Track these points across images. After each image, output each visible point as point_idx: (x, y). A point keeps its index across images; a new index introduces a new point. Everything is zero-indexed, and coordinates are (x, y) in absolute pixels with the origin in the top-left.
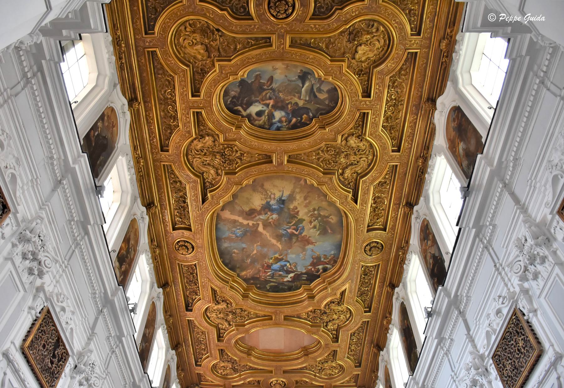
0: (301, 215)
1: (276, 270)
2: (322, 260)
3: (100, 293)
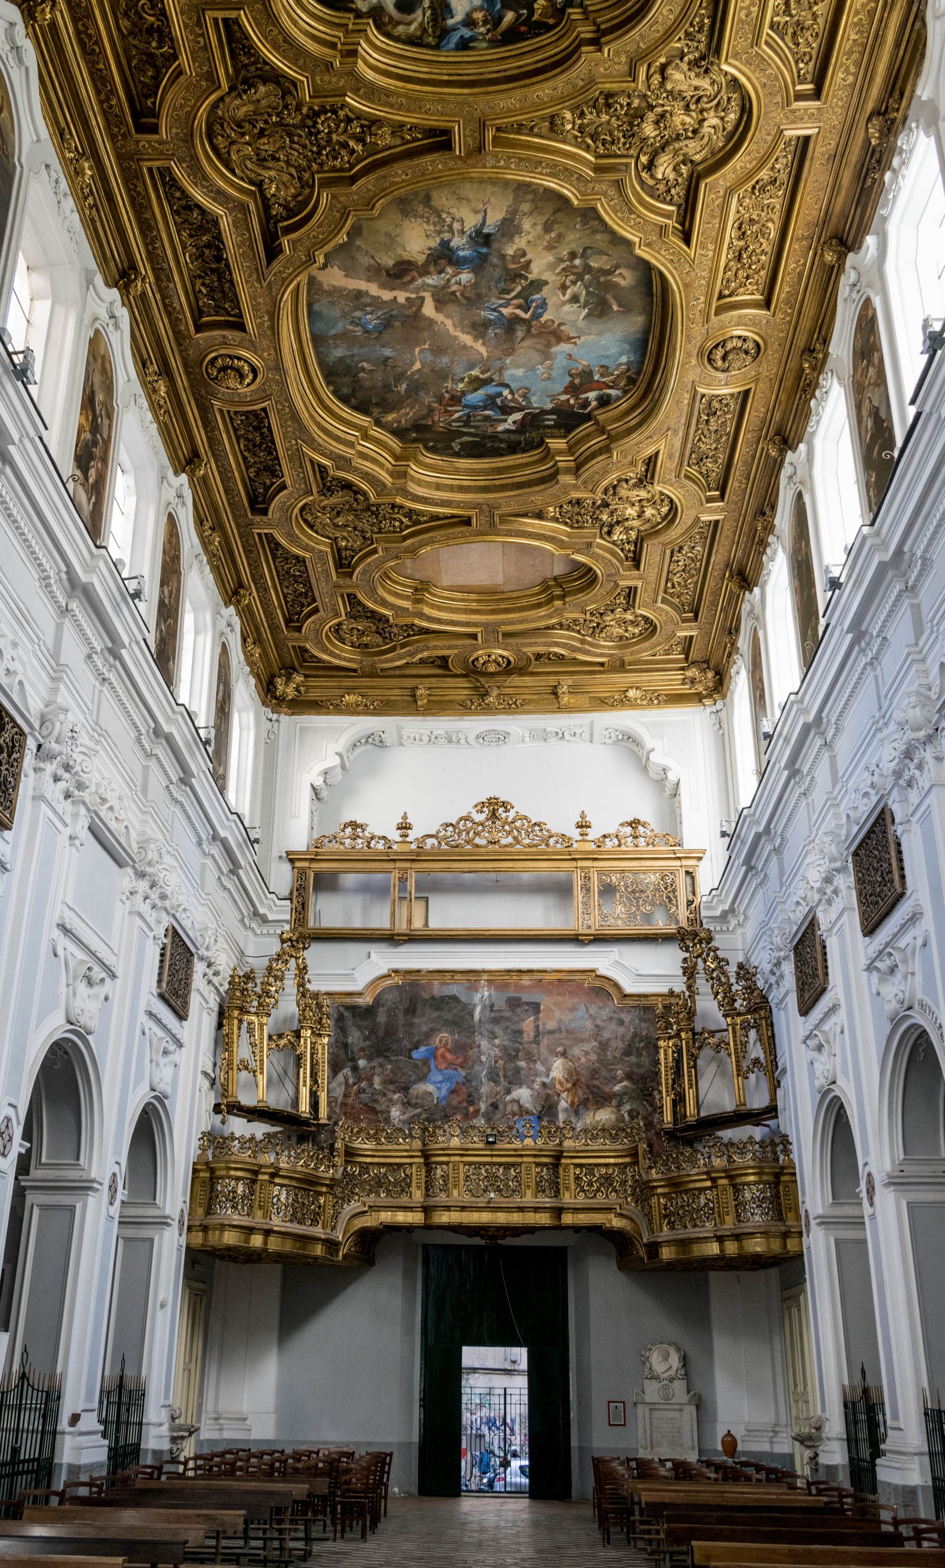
1: (475, 408)
2: (596, 377)
3: (58, 574)
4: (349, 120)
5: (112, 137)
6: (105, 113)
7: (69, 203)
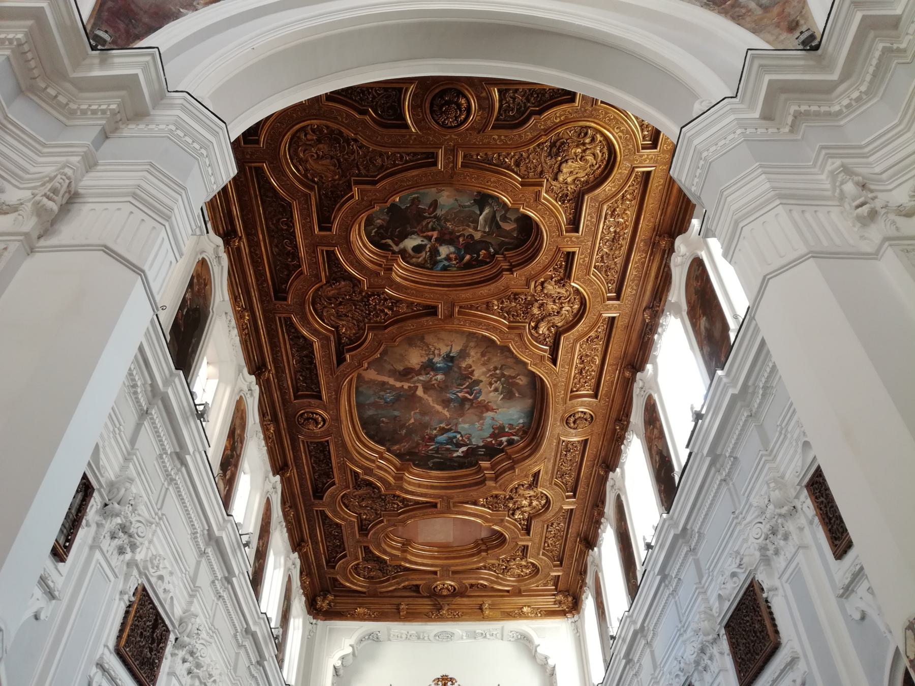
0: (477, 375)
1: (441, 443)
4: (386, 300)
5: (262, 302)
6: (259, 290)
7: (235, 332)
